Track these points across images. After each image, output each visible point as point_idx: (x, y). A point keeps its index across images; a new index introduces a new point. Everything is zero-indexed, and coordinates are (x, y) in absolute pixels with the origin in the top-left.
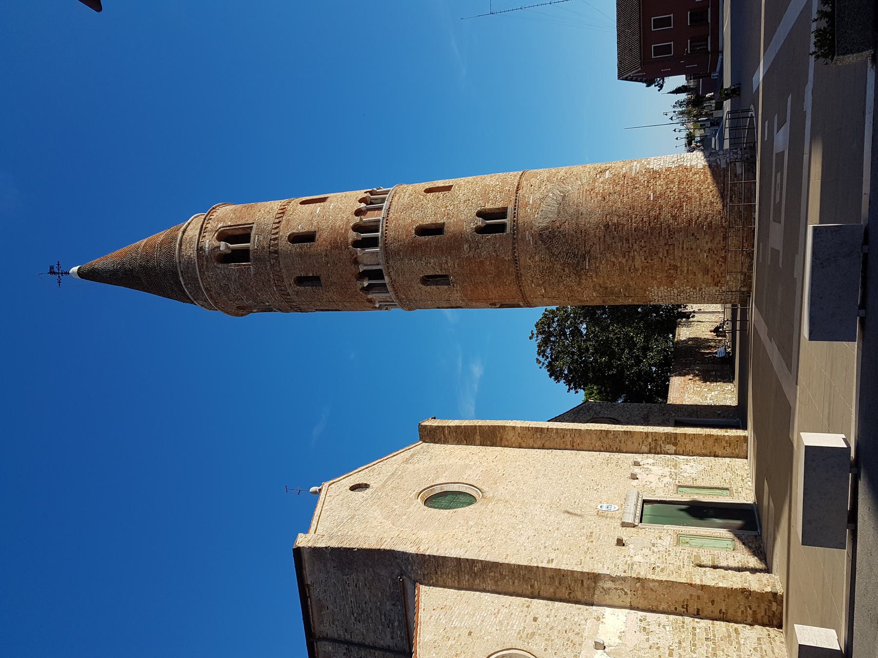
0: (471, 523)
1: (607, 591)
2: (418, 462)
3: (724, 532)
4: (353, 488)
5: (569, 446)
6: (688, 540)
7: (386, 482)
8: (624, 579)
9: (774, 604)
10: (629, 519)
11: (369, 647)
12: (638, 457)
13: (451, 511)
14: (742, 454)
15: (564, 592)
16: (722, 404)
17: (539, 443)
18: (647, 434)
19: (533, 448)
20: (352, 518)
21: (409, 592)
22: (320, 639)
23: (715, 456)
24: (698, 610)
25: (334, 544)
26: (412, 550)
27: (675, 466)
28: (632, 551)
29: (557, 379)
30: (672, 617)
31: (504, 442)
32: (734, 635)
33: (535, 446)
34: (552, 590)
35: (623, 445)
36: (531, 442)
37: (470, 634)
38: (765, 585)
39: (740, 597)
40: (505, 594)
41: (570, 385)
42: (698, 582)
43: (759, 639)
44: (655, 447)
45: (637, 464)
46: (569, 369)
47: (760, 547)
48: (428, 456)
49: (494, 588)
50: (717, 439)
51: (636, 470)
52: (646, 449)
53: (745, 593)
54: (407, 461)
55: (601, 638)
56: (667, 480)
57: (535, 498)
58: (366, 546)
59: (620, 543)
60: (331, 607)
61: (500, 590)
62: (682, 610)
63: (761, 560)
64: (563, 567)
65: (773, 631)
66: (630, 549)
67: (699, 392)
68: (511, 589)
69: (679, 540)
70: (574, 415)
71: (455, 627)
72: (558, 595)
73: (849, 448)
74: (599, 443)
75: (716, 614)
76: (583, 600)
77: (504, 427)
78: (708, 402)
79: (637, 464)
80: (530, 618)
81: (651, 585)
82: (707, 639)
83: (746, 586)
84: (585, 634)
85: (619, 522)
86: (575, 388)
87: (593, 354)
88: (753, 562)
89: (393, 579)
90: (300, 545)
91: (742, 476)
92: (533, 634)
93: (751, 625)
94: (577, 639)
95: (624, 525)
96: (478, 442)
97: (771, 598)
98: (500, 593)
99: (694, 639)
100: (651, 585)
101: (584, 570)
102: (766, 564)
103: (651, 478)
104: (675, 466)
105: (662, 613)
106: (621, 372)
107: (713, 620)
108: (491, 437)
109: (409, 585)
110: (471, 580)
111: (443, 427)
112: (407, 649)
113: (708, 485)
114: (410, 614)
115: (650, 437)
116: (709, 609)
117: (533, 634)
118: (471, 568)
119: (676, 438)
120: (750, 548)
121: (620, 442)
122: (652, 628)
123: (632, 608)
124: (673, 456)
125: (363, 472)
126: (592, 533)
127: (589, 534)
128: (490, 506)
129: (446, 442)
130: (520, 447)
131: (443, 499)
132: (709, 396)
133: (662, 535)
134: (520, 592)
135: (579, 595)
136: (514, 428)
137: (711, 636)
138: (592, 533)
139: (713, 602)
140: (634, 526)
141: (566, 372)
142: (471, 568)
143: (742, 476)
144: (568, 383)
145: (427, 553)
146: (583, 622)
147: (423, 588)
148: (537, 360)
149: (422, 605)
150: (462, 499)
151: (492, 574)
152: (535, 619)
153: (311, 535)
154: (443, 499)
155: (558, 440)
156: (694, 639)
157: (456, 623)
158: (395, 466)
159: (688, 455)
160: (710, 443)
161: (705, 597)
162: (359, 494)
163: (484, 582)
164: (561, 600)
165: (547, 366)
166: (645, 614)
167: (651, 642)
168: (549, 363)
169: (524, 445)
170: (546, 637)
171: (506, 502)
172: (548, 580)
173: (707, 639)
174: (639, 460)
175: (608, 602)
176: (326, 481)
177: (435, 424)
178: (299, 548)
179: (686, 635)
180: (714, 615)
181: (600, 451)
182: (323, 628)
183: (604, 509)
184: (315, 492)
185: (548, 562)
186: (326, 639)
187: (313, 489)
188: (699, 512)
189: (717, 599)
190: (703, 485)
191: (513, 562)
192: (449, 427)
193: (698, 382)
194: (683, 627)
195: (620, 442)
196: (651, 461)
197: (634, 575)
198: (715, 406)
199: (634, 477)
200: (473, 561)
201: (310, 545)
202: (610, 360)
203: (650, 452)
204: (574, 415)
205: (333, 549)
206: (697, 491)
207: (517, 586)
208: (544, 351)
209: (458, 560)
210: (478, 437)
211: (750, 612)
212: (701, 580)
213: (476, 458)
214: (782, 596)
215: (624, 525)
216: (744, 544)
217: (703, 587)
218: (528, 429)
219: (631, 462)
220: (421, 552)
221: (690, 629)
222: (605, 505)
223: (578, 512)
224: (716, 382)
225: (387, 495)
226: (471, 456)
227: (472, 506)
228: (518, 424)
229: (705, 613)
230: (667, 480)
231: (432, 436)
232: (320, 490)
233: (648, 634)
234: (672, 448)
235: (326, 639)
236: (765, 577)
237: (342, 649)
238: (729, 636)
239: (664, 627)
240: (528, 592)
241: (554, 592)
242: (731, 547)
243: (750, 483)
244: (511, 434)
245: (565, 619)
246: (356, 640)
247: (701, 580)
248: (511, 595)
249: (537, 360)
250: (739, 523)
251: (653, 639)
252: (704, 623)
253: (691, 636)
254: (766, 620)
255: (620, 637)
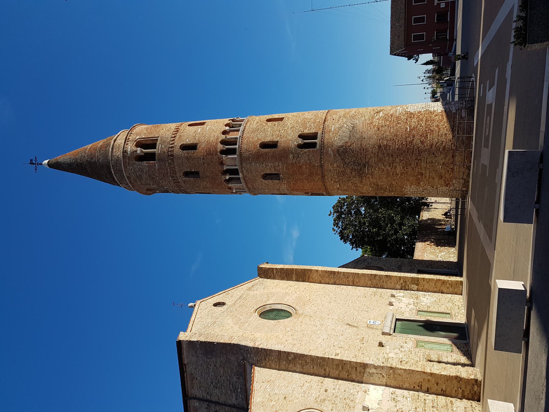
0: (288, 329)
1: (371, 375)
2: (256, 290)
3: (446, 341)
4: (216, 305)
5: (351, 284)
6: (423, 344)
7: (236, 302)
8: (382, 367)
9: (476, 386)
10: (387, 330)
11: (222, 404)
12: (394, 292)
13: (276, 321)
14: (459, 292)
15: (344, 374)
16: (447, 260)
17: (332, 281)
18: (400, 277)
19: (328, 284)
20: (214, 323)
21: (248, 370)
22: (191, 398)
23: (442, 293)
24: (428, 388)
25: (202, 339)
26: (250, 344)
27: (417, 298)
28: (388, 350)
29: (345, 241)
30: (411, 392)
31: (311, 280)
32: (450, 405)
33: (330, 282)
34: (337, 373)
35: (385, 284)
36: (327, 280)
37: (285, 398)
38: (470, 375)
39: (455, 381)
40: (308, 374)
41: (353, 245)
42: (429, 371)
43: (465, 408)
44: (405, 286)
45: (393, 296)
46: (353, 235)
47: (468, 350)
48: (263, 287)
49: (301, 370)
50: (444, 282)
51: (393, 300)
52: (399, 287)
53: (458, 379)
54: (249, 289)
55: (367, 404)
56: (412, 306)
57: (328, 315)
58: (222, 341)
59: (381, 345)
60: (199, 378)
61: (305, 371)
62: (418, 388)
63: (468, 358)
64: (345, 359)
65: (474, 403)
66: (387, 349)
67: (434, 252)
68: (312, 372)
69: (418, 344)
70: (355, 264)
71: (276, 394)
72: (341, 376)
73: (526, 290)
74: (370, 282)
75: (439, 391)
76: (356, 380)
77: (311, 270)
78: (439, 259)
79: (393, 296)
80: (323, 390)
81: (399, 371)
82: (433, 407)
83: (458, 374)
84: (357, 401)
85: (381, 332)
86: (356, 248)
87: (368, 226)
88: (464, 360)
89: (238, 362)
90: (181, 339)
91: (459, 306)
92: (324, 400)
93: (460, 399)
94: (352, 404)
95: (384, 334)
96: (294, 279)
97: (474, 382)
98: (304, 374)
99: (425, 407)
100: (399, 371)
101: (358, 361)
102: (471, 361)
103: (402, 305)
104: (417, 298)
105: (405, 389)
106: (385, 239)
107: (437, 395)
108: (302, 276)
109: (248, 366)
110: (287, 365)
111: (273, 269)
112: (246, 407)
113: (437, 311)
114: (248, 385)
115: (402, 279)
116: (435, 388)
117: (324, 400)
118: (287, 357)
119: (418, 281)
120: (462, 351)
121: (383, 282)
122: (399, 399)
123: (386, 386)
124: (416, 292)
125: (222, 295)
126: (363, 338)
127: (361, 338)
128: (300, 319)
129: (274, 278)
130: (320, 283)
131: (271, 313)
132: (440, 255)
133: (407, 341)
134: (317, 373)
135: (354, 376)
136: (317, 271)
137: (435, 405)
138: (363, 338)
139: (437, 384)
140: (390, 335)
141: (351, 237)
142: (287, 357)
143: (459, 306)
144: (352, 244)
145: (260, 347)
146: (356, 393)
147: (257, 368)
148: (333, 229)
149: (255, 379)
150: (283, 314)
151: (300, 361)
152: (326, 391)
153: (188, 333)
154: (271, 313)
155: (344, 279)
156: (425, 407)
157: (277, 391)
158: (242, 292)
159: (425, 291)
160: (439, 284)
161: (433, 380)
162: (219, 309)
163: (295, 366)
164: (343, 379)
165: (339, 233)
166: (395, 389)
167: (398, 408)
168: (341, 231)
169: (323, 281)
170: (333, 402)
171: (311, 317)
172: (335, 367)
173: (433, 407)
174: (394, 293)
175: (372, 381)
176: (199, 300)
177: (268, 267)
178: (180, 341)
179: (420, 404)
180: (437, 392)
181: (370, 287)
182: (193, 391)
183: (372, 323)
184: (192, 307)
185: (335, 355)
186: (195, 398)
187: (190, 304)
188: (431, 327)
189: (440, 382)
190: (434, 310)
191: (313, 354)
192: (276, 269)
193: (433, 247)
194: (418, 399)
195: (383, 282)
196: (402, 294)
197: (389, 365)
198: (443, 261)
199: (391, 304)
200: (289, 353)
201: (187, 339)
202: (378, 230)
203: (401, 289)
204: (355, 264)
205: (201, 342)
206: (431, 314)
207: (316, 370)
208: (337, 224)
209: (279, 352)
210: (294, 276)
211: (460, 391)
212: (431, 370)
213: (292, 289)
214: (481, 382)
215: (384, 334)
216: (458, 348)
217: (431, 374)
218: (326, 272)
219: (389, 294)
220: (256, 346)
221: (423, 400)
222: (372, 321)
223: (355, 325)
224: (445, 246)
225: (236, 310)
226: (289, 287)
227: (289, 319)
228: (320, 268)
229: (433, 391)
230: (412, 306)
231: (266, 274)
232: (195, 305)
233: (396, 402)
234: (416, 287)
235: (195, 398)
236: (470, 369)
237: (205, 405)
238: (447, 405)
239: (406, 398)
240: (322, 374)
241: (339, 374)
242: (450, 350)
243: (463, 311)
244: (315, 274)
245: (345, 391)
246: (215, 399)
247: (431, 370)
248: (312, 375)
249: (333, 229)
250: (455, 335)
251: (399, 406)
252: (431, 397)
253: (423, 405)
254: (470, 396)
255: (379, 404)
